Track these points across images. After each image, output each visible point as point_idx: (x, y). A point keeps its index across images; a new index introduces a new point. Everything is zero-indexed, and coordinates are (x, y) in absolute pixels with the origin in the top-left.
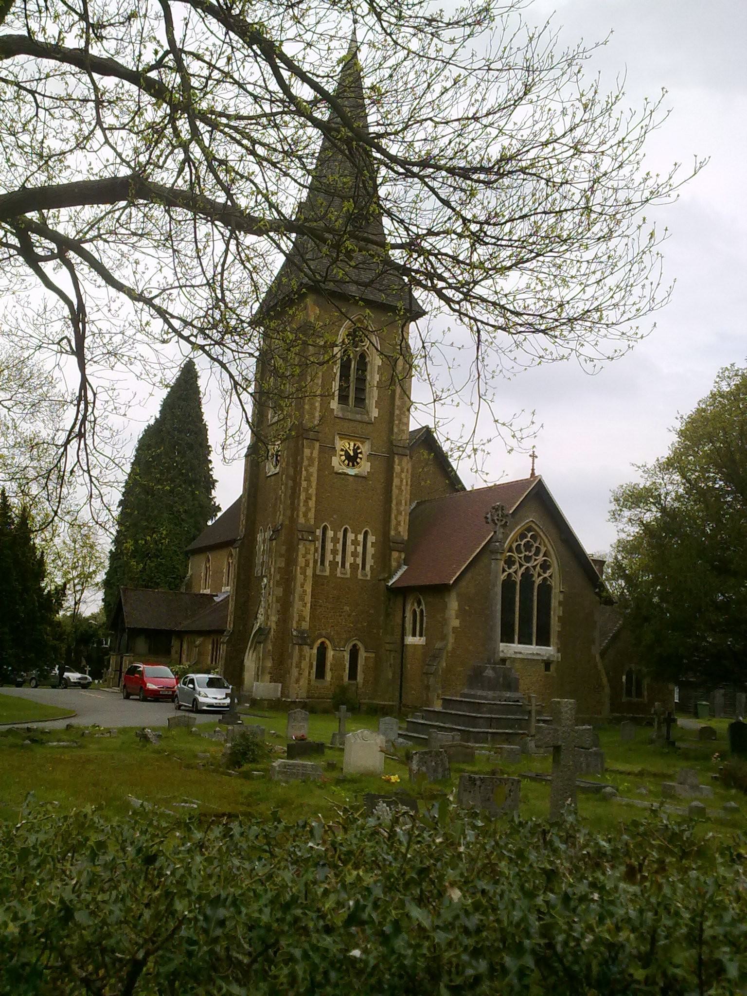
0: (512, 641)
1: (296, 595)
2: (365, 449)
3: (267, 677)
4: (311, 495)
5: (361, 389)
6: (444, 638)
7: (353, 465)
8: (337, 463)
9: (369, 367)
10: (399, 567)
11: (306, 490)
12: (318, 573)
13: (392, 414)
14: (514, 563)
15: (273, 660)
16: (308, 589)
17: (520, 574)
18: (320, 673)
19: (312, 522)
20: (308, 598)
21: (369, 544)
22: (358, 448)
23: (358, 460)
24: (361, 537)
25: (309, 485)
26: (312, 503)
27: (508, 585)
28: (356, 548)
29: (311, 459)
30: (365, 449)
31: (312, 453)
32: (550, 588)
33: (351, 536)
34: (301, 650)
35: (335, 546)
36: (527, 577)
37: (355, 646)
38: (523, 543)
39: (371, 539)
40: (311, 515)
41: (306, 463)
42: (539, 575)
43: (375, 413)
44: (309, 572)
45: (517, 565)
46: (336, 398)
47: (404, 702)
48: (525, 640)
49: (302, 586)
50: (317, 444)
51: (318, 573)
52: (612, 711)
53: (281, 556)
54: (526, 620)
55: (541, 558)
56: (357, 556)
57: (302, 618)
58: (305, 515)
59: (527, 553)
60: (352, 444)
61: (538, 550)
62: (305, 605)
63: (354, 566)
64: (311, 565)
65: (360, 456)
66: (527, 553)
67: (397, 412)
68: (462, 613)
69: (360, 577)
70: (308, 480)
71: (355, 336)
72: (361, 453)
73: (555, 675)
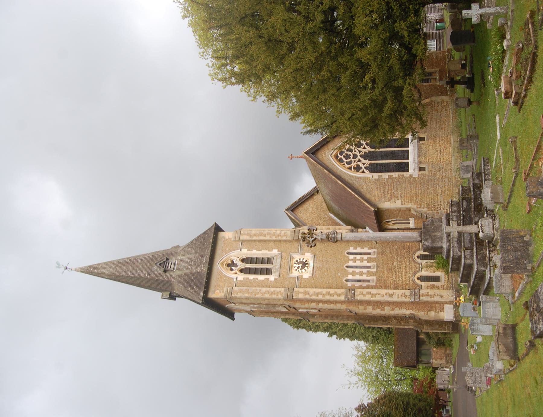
0: (407, 164)
2: (297, 257)
4: (327, 292)
5: (262, 261)
6: (409, 210)
7: (307, 264)
8: (306, 274)
9: (249, 256)
11: (324, 295)
12: (374, 284)
13: (275, 241)
14: (358, 166)
15: (430, 311)
16: (384, 292)
17: (364, 161)
18: (437, 279)
19: (343, 290)
20: (391, 291)
21: (355, 251)
22: (297, 261)
23: (304, 261)
24: (351, 257)
25: (321, 293)
26: (332, 291)
27: (373, 169)
28: (358, 260)
29: (305, 293)
30: (297, 257)
31: (301, 293)
33: (351, 263)
34: (423, 295)
35: (357, 274)
36: (366, 156)
37: (418, 257)
38: (345, 160)
39: (352, 250)
40: (339, 291)
41: (307, 297)
42: (364, 148)
43: (275, 251)
44: (374, 291)
45: (359, 163)
48: (405, 154)
49: (383, 296)
51: (374, 284)
54: (393, 155)
56: (363, 258)
57: (403, 295)
58: (339, 295)
59: (351, 157)
60: (295, 265)
62: (395, 293)
63: (369, 260)
64: (369, 290)
65: (301, 260)
66: (351, 157)
67: (274, 238)
68: (392, 198)
69: (375, 256)
70: (317, 294)
71: (231, 265)
72: (300, 259)
73: (426, 134)
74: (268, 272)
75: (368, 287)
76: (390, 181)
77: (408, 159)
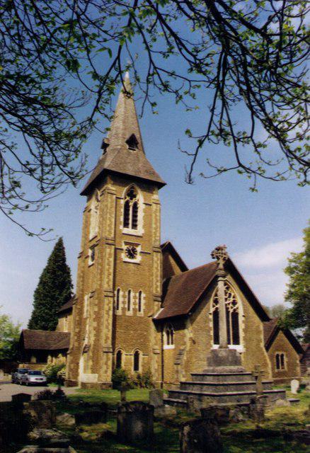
1: (104, 326)
3: (90, 371)
5: (135, 221)
10: (158, 310)
24: (137, 295)
32: (237, 314)
33: (132, 294)
41: (107, 256)
46: (122, 224)
47: (165, 380)
50: (113, 247)
52: (273, 377)
53: (96, 305)
55: (232, 299)
61: (230, 294)
64: (112, 309)
74: (126, 225)
75: (114, 308)
76: (207, 328)
77: (234, 344)
